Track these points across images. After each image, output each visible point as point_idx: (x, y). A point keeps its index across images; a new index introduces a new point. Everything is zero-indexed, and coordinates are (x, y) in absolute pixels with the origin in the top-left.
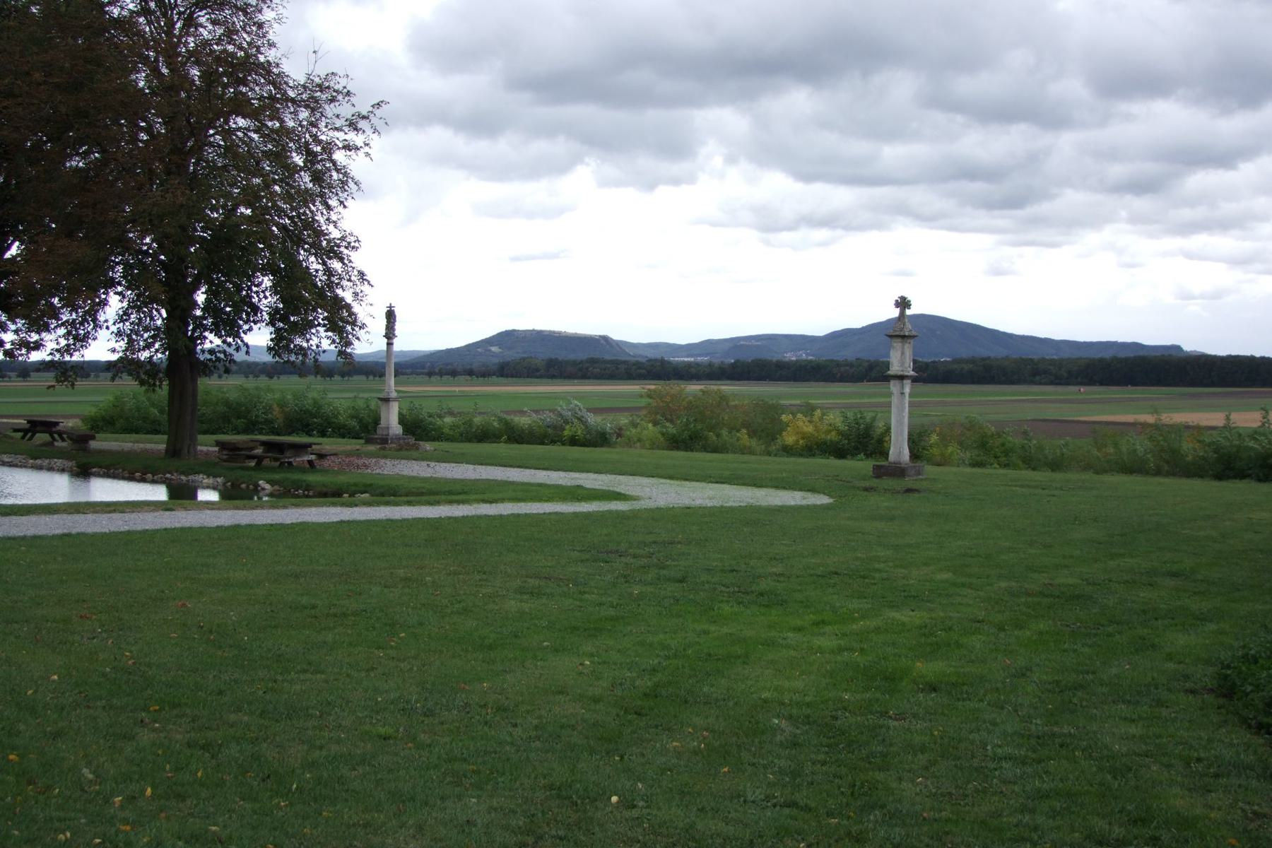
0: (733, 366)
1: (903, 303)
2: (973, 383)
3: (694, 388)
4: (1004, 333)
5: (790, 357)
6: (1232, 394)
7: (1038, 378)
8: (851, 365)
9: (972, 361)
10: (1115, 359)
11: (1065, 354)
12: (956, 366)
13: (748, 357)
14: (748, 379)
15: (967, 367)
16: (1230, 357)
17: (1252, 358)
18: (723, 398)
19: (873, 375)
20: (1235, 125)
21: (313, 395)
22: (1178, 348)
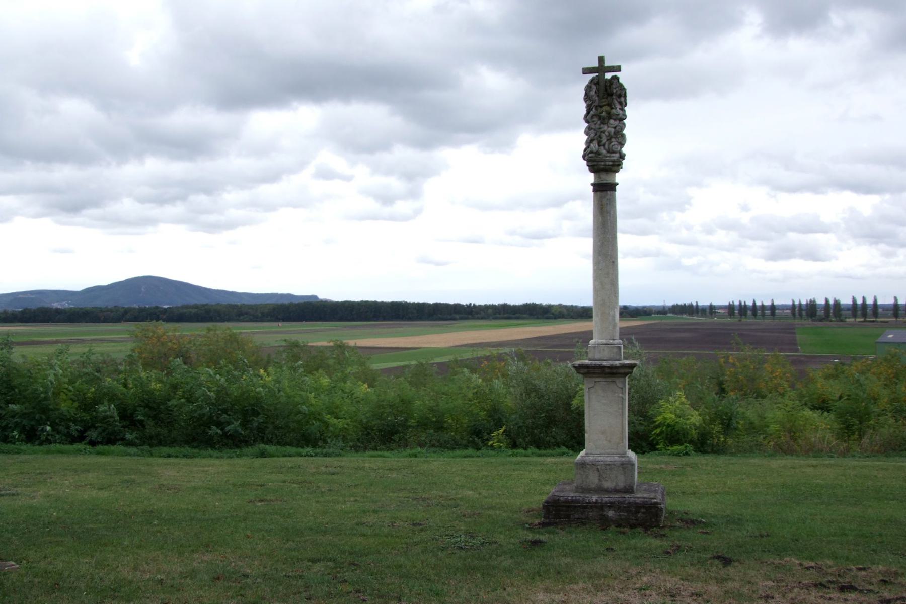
0: (24, 312)
1: (896, 298)
2: (198, 321)
3: (759, 334)
4: (205, 289)
5: (56, 305)
6: (364, 326)
7: (242, 317)
8: (111, 311)
9: (196, 306)
10: (291, 304)
11: (302, 301)
12: (185, 310)
13: (33, 306)
14: (35, 321)
15: (193, 311)
16: (362, 302)
17: (376, 303)
18: (233, 339)
19: (128, 317)
20: (153, 211)
21: (77, 350)
22: (316, 297)
